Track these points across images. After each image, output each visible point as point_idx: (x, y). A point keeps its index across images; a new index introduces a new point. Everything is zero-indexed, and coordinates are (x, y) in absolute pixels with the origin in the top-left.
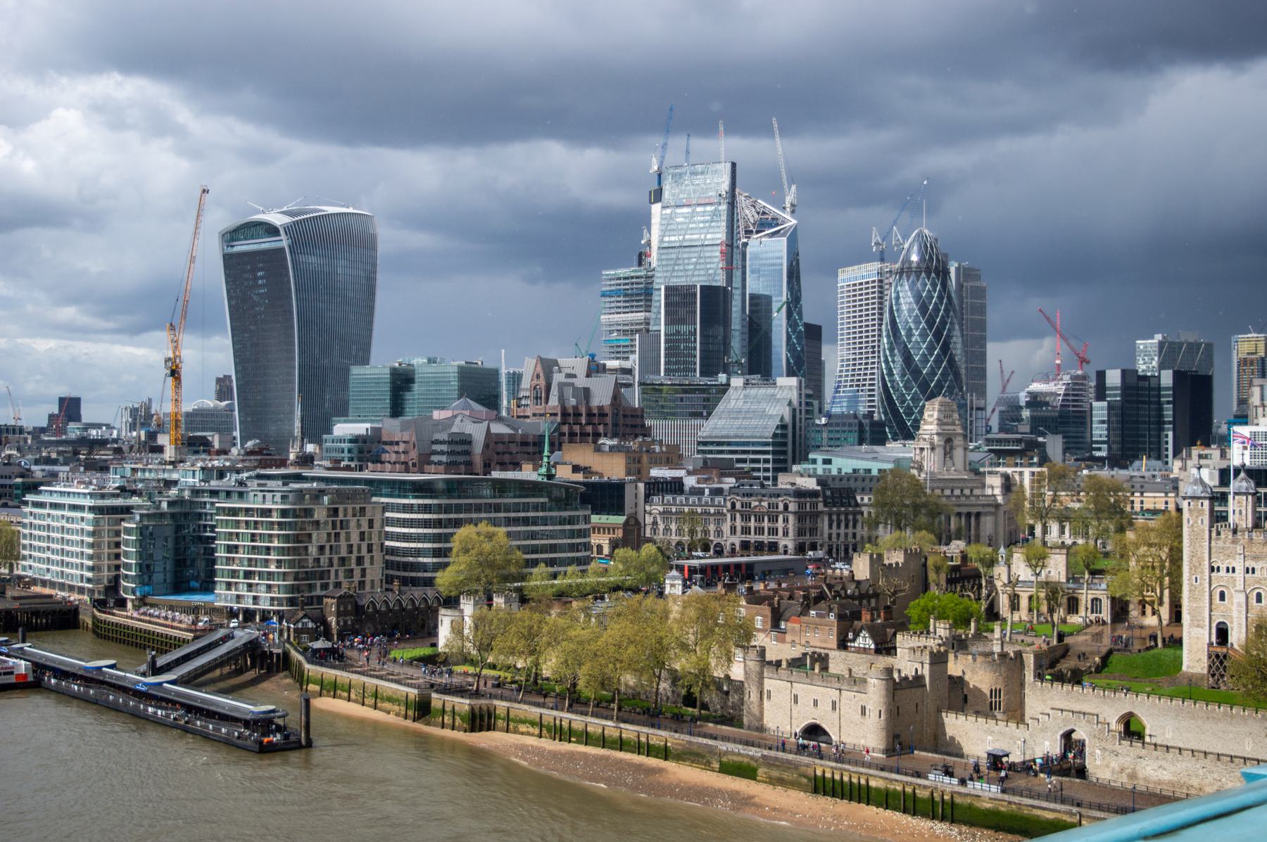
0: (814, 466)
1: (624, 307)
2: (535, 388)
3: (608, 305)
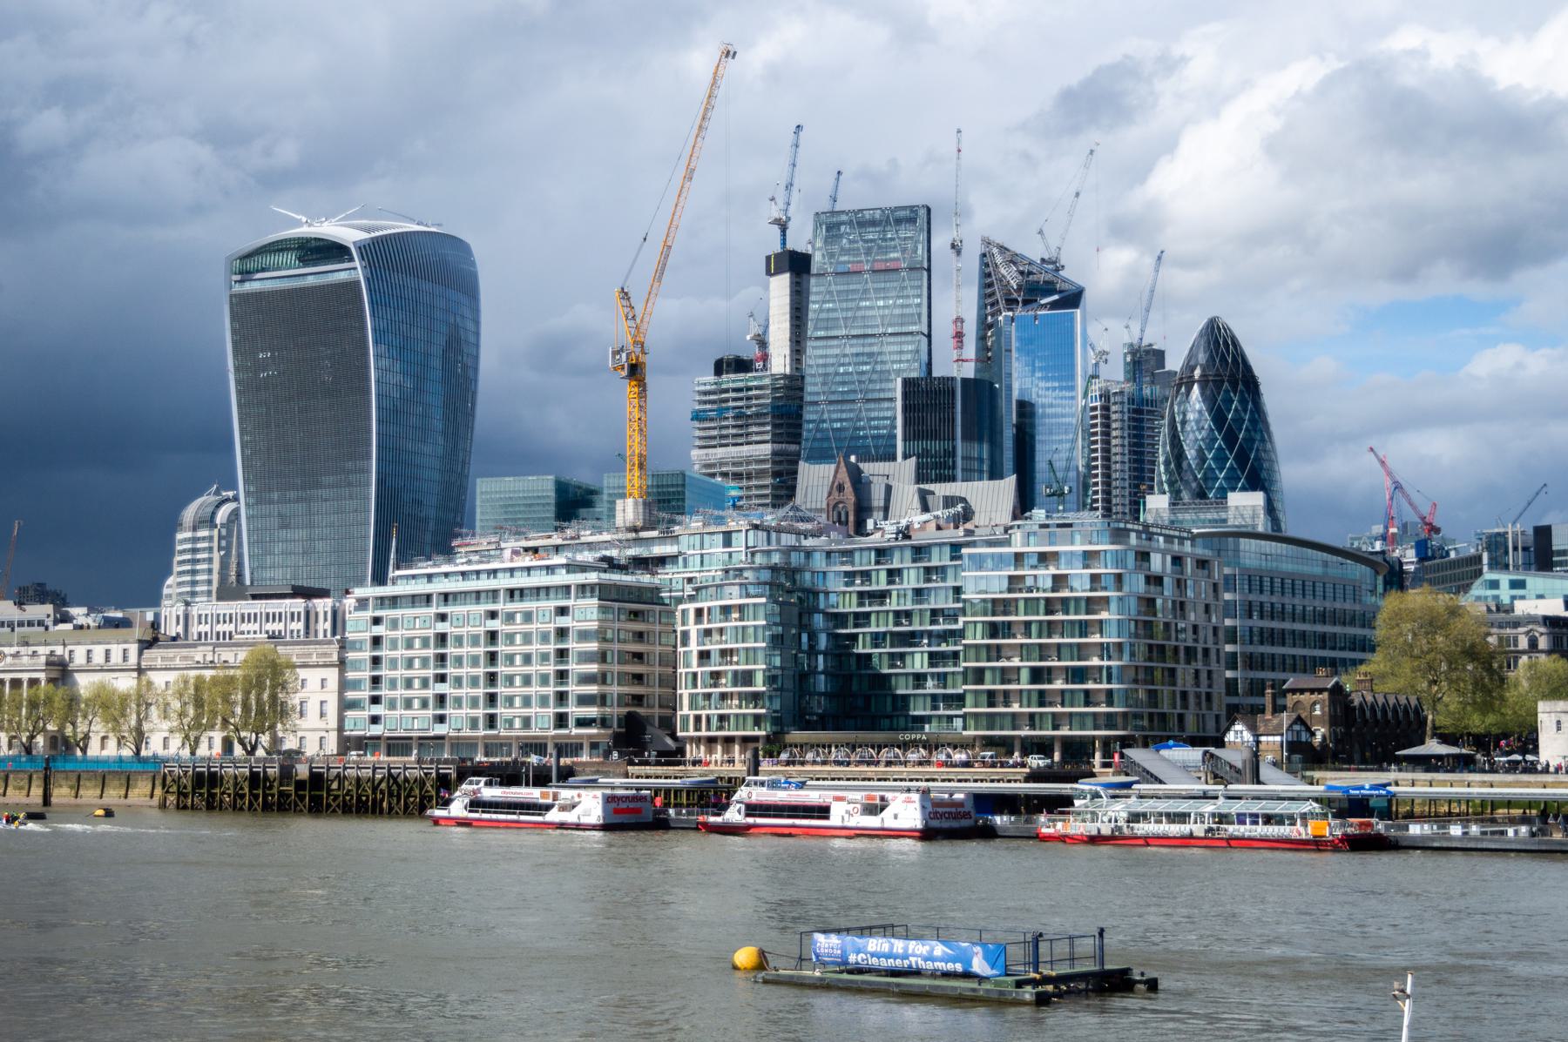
0: (1495, 592)
1: (735, 436)
2: (835, 506)
3: (698, 433)
